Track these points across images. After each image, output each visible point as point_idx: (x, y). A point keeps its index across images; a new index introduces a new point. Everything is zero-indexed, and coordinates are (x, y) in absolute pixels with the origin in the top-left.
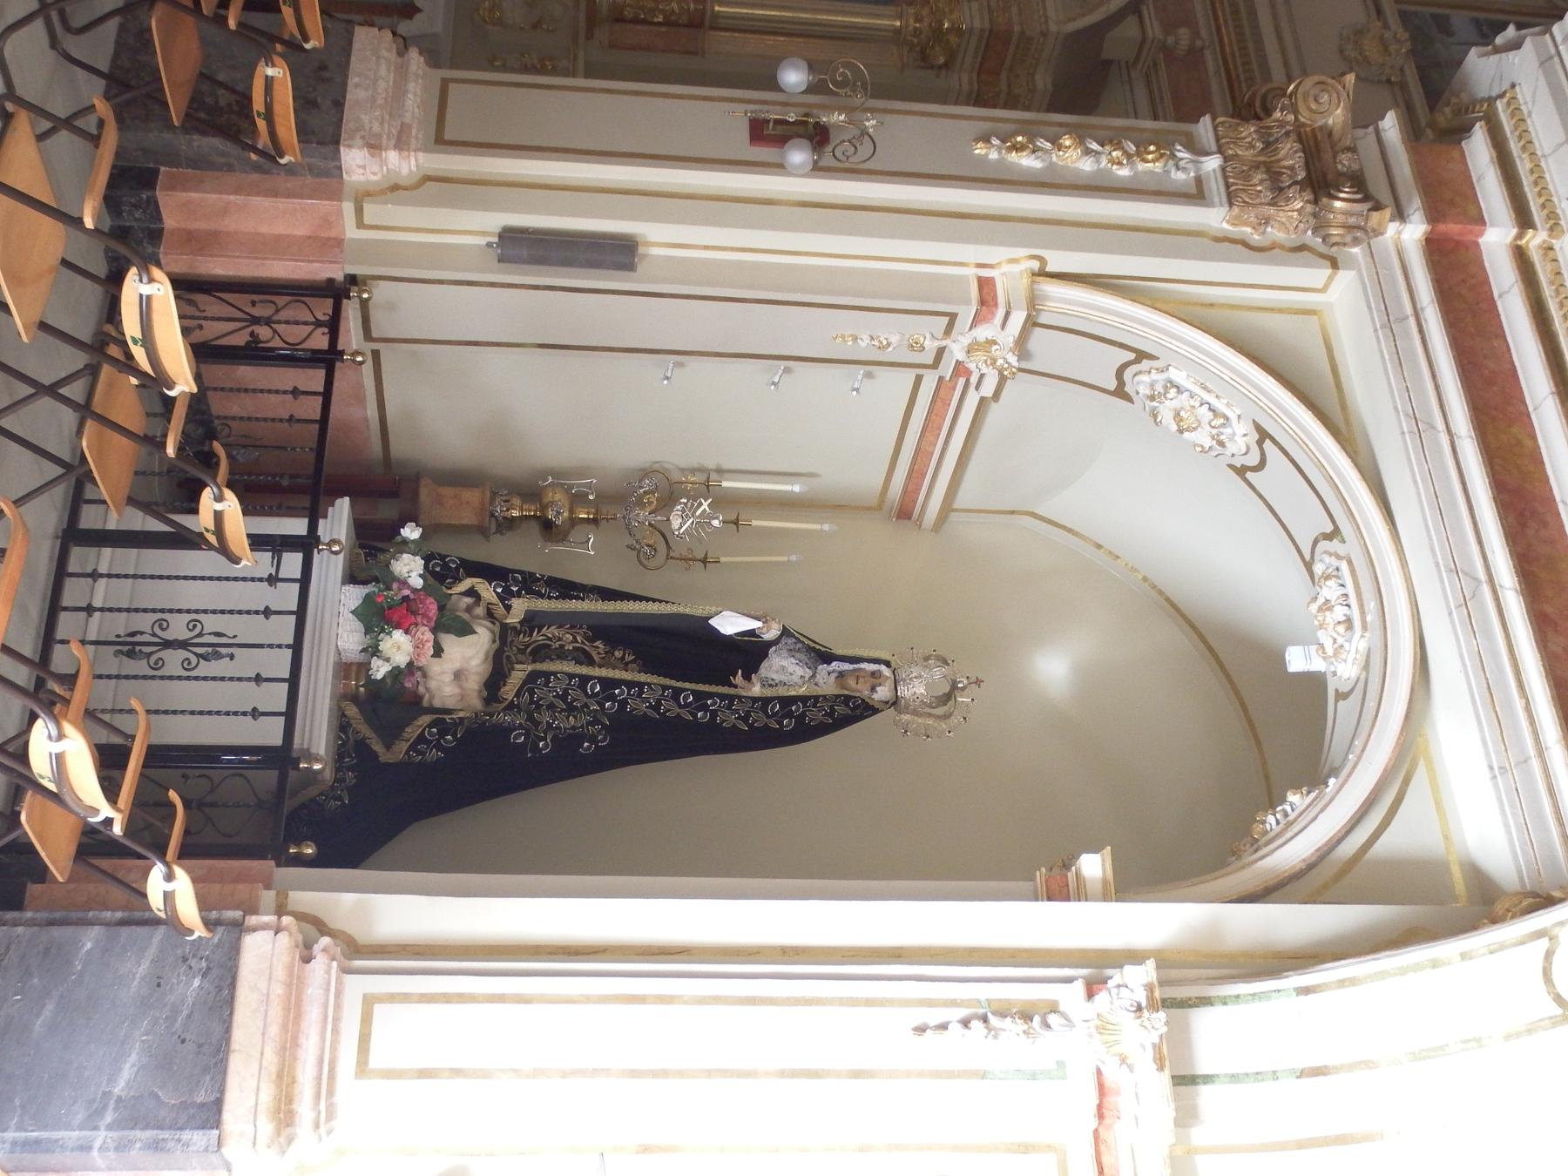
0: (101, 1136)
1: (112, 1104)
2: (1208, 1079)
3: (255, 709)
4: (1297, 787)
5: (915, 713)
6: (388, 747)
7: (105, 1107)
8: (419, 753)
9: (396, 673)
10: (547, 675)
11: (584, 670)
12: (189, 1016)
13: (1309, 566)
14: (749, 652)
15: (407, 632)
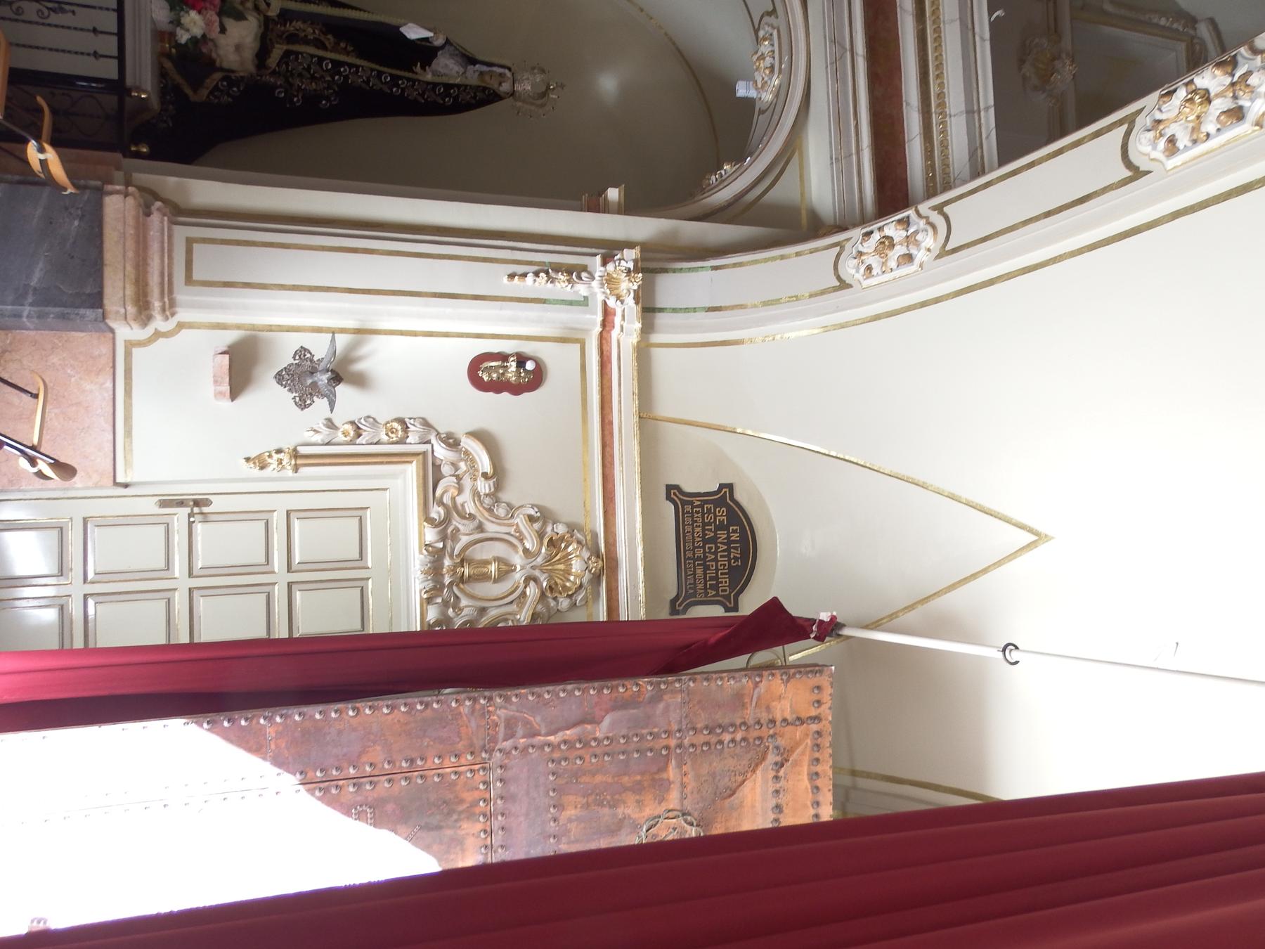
0: (27, 310)
1: (31, 292)
2: (661, 310)
3: (95, 53)
4: (729, 161)
5: (524, 101)
6: (195, 91)
7: (26, 293)
8: (216, 97)
9: (194, 40)
10: (297, 53)
11: (321, 53)
12: (74, 243)
13: (756, 32)
14: (425, 52)
15: (199, 12)
